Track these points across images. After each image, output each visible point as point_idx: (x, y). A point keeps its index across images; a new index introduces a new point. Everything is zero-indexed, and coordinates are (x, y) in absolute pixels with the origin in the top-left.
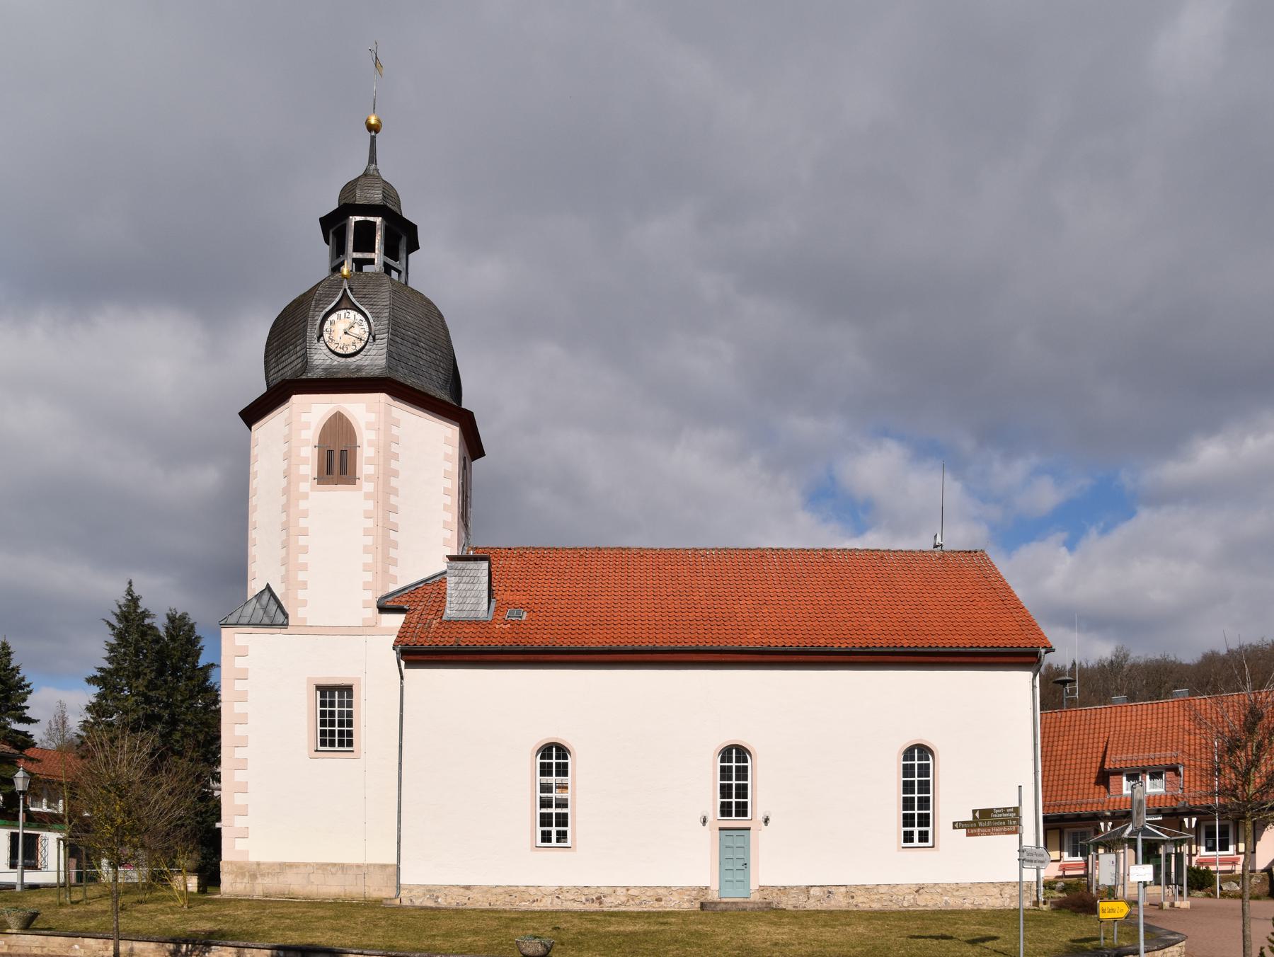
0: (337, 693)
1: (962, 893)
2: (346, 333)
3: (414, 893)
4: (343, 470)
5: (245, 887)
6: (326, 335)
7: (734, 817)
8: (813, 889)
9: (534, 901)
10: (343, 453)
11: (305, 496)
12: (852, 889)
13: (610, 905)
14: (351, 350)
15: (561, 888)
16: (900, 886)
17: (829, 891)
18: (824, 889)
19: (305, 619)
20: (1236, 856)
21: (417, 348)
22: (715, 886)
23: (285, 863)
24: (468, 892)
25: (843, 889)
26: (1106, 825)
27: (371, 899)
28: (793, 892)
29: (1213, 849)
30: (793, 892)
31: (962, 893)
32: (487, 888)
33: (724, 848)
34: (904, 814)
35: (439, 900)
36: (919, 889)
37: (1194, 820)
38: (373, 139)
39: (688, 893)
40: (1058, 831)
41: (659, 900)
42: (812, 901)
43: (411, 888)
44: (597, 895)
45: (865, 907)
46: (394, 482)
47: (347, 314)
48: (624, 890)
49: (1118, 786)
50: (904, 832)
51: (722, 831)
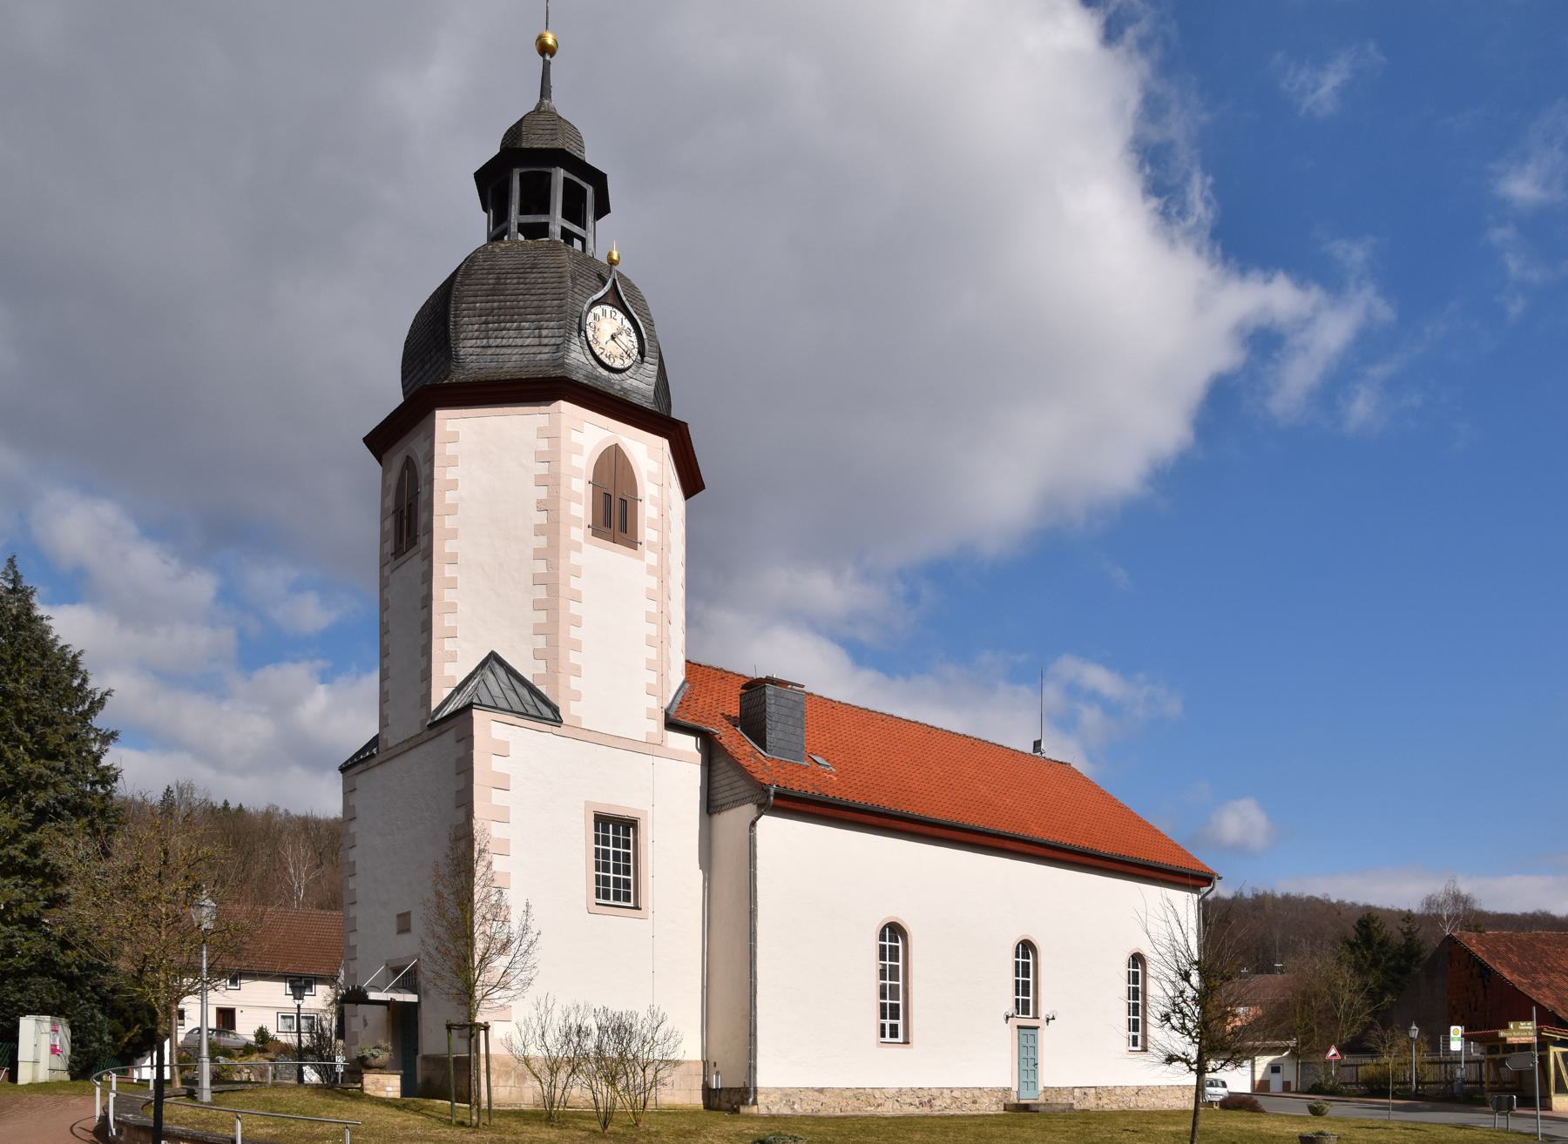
0: (611, 826)
3: (771, 1098)
5: (510, 1093)
9: (878, 1106)
11: (577, 547)
14: (618, 364)
15: (900, 1089)
27: (663, 1107)
32: (838, 1091)
33: (908, 1039)
35: (796, 1107)
36: (1139, 1091)
41: (974, 1102)
45: (1107, 1108)
47: (613, 314)
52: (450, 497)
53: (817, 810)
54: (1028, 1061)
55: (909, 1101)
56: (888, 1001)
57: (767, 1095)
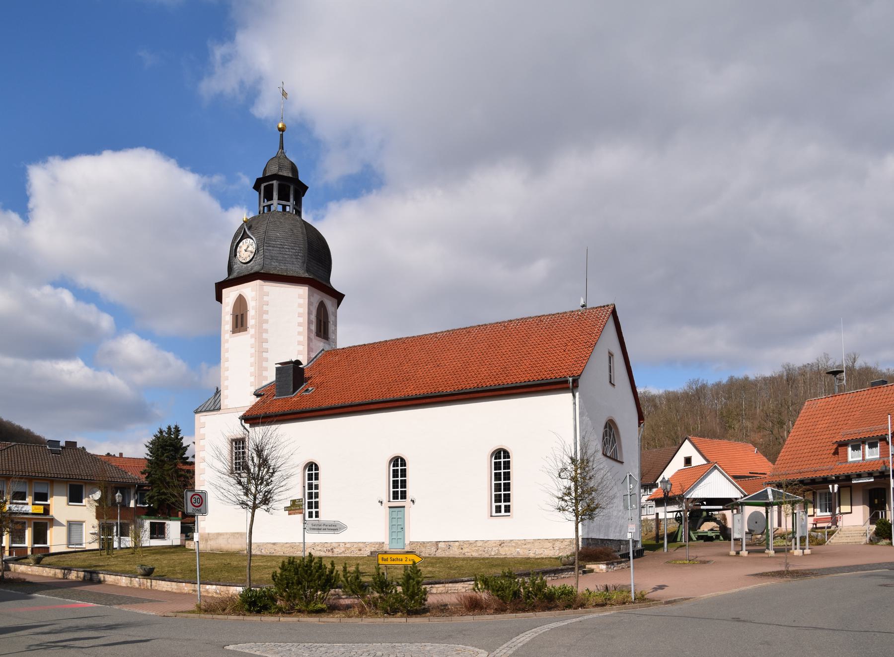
1: (528, 546)
2: (246, 251)
4: (242, 325)
6: (238, 254)
7: (399, 500)
8: (441, 543)
10: (242, 315)
12: (462, 544)
13: (337, 553)
15: (315, 543)
16: (490, 542)
17: (449, 544)
18: (446, 543)
19: (227, 405)
21: (283, 249)
22: (387, 541)
24: (274, 547)
25: (457, 544)
26: (833, 487)
28: (428, 545)
30: (428, 545)
31: (528, 546)
33: (392, 519)
34: (509, 491)
36: (501, 544)
38: (282, 136)
39: (374, 546)
40: (849, 488)
41: (360, 550)
42: (439, 551)
43: (259, 546)
44: (332, 547)
45: (468, 555)
46: (265, 326)
48: (343, 544)
49: (845, 455)
50: (496, 506)
51: (391, 509)
52: (301, 320)
53: (293, 416)
54: (397, 525)
56: (314, 500)
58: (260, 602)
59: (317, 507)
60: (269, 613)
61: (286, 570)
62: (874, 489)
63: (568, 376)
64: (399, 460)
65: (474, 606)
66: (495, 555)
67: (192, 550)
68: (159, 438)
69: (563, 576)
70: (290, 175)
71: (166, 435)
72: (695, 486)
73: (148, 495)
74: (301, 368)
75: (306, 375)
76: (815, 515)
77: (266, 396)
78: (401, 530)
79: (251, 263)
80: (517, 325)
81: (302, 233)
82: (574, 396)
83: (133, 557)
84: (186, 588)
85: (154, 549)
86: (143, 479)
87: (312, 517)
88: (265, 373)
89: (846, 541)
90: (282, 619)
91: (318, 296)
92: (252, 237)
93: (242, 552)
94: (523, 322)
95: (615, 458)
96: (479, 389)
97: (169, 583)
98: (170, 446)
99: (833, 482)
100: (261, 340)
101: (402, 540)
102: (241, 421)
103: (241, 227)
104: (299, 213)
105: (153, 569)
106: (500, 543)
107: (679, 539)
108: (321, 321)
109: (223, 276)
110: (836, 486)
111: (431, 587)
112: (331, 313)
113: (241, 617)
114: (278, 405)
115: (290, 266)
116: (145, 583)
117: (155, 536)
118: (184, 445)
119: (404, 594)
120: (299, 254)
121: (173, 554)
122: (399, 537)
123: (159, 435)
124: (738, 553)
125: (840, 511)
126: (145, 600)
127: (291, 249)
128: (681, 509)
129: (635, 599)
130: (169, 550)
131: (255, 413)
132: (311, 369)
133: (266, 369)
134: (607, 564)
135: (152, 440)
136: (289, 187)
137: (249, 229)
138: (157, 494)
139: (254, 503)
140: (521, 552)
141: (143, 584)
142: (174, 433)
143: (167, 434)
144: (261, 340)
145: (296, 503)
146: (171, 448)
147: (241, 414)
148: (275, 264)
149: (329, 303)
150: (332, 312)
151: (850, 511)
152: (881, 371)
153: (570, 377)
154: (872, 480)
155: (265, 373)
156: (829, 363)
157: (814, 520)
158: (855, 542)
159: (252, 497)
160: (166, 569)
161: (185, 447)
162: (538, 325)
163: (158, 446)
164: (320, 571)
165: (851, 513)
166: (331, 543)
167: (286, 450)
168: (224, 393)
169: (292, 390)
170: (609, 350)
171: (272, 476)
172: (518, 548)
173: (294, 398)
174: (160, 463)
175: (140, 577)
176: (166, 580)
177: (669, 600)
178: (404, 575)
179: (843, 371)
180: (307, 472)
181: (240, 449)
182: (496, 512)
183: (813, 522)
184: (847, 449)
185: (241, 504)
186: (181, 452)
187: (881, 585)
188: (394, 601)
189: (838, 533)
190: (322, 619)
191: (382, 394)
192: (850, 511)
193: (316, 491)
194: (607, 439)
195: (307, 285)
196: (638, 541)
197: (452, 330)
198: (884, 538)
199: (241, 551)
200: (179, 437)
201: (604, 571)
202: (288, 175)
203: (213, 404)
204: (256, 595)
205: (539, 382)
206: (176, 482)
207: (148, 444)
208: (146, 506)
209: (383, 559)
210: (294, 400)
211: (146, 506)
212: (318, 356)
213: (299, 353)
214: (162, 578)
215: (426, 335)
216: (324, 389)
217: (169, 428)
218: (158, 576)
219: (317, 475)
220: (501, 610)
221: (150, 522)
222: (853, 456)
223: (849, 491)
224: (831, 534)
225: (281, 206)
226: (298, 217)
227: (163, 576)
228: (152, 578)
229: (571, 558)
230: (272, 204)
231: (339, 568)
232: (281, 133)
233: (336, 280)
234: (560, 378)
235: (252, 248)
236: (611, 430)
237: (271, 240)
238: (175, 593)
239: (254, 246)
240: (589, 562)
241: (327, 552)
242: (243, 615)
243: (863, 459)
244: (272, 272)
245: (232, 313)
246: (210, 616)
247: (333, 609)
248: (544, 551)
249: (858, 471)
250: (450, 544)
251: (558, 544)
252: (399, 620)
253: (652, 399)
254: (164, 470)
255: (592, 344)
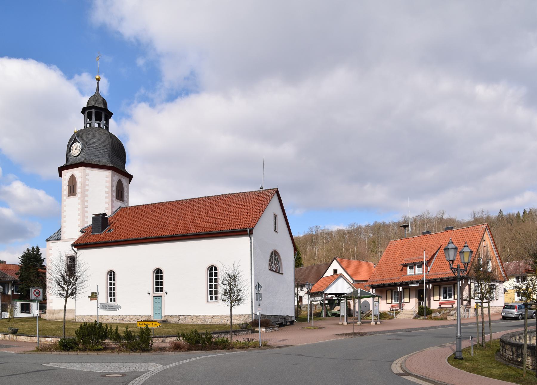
2: (76, 149)
3: (79, 318)
4: (73, 192)
6: (71, 151)
8: (181, 316)
15: (113, 316)
16: (207, 316)
17: (185, 317)
19: (65, 237)
20: (454, 301)
22: (152, 315)
23: (60, 310)
24: (91, 317)
25: (190, 317)
26: (400, 288)
29: (446, 298)
33: (155, 303)
36: (213, 317)
37: (431, 285)
38: (98, 83)
40: (409, 289)
42: (180, 320)
43: (78, 316)
45: (196, 323)
46: (86, 193)
48: (129, 316)
52: (107, 190)
54: (158, 306)
55: (116, 319)
56: (113, 292)
57: (78, 317)
58: (69, 345)
59: (114, 296)
60: (74, 351)
61: (82, 329)
62: (420, 290)
63: (247, 228)
64: (159, 270)
65: (177, 347)
66: (209, 323)
67: (45, 319)
68: (27, 253)
69: (239, 334)
70: (103, 107)
71: (31, 252)
72: (330, 287)
73: (20, 287)
74: (106, 217)
75: (109, 221)
76: (440, 300)
77: (87, 233)
78: (160, 309)
79: (79, 156)
80: (226, 198)
81: (109, 140)
82: (251, 238)
83: (8, 324)
84: (35, 340)
85: (22, 319)
86: (17, 278)
87: (112, 301)
88: (86, 220)
89: (404, 317)
90: (79, 353)
91: (117, 177)
92: (79, 141)
93: (73, 321)
94: (229, 196)
95: (278, 271)
96: (201, 233)
97: (26, 337)
98: (34, 259)
99: (399, 286)
100: (84, 201)
101: (160, 314)
102: (72, 247)
103: (73, 136)
104: (107, 128)
105: (18, 330)
106: (212, 317)
107: (322, 316)
108: (119, 190)
109: (63, 163)
110: (401, 288)
111: (165, 339)
112: (125, 186)
113: (59, 353)
114: (94, 238)
115: (101, 159)
116: (13, 337)
117: (24, 311)
118: (42, 258)
119: (140, 341)
120: (107, 152)
121: (33, 322)
122: (159, 313)
123: (27, 252)
124: (376, 323)
125: (404, 301)
126: (11, 346)
127: (102, 149)
128: (322, 299)
129: (261, 345)
130: (31, 319)
131: (79, 242)
132: (113, 218)
133: (87, 217)
134: (266, 328)
135: (22, 255)
136: (102, 113)
137: (78, 137)
138: (25, 287)
139: (67, 295)
140: (223, 321)
141: (12, 338)
142: (36, 251)
143: (31, 251)
144: (84, 201)
145: (94, 294)
146: (34, 260)
147: (72, 242)
148: (92, 158)
149: (124, 181)
150: (126, 185)
151: (409, 301)
152: (459, 221)
153: (248, 228)
154: (418, 285)
155: (86, 220)
156: (429, 216)
157: (392, 306)
158: (408, 318)
159: (66, 292)
160: (26, 330)
161: (43, 259)
162: (236, 198)
163: (26, 258)
164: (100, 329)
165: (409, 302)
166: (123, 316)
167: (83, 268)
168: (63, 230)
169: (101, 230)
170: (274, 213)
171: (76, 281)
172: (222, 319)
173: (102, 234)
174: (28, 269)
175: (10, 334)
176: (25, 335)
177: (278, 346)
178: (140, 331)
179: (409, 226)
180: (109, 276)
181: (72, 262)
182: (211, 300)
183: (391, 307)
184: (407, 268)
185: (59, 295)
186: (40, 262)
187: (389, 339)
188: (135, 344)
189: (401, 313)
190: (99, 353)
191: (150, 234)
192: (409, 301)
193: (114, 287)
194: (273, 261)
195: (111, 170)
196: (293, 316)
197: (191, 199)
198: (422, 316)
199: (72, 320)
200: (39, 254)
201: (264, 332)
202: (101, 107)
203: (57, 237)
204: (67, 341)
205: (232, 230)
206: (37, 280)
207: (20, 257)
208: (19, 293)
209: (140, 324)
210: (103, 235)
211: (19, 293)
212: (117, 211)
213: (106, 208)
214: (23, 335)
215: (177, 201)
216: (119, 230)
217: (33, 248)
218: (21, 334)
219: (114, 278)
220: (189, 349)
221: (21, 303)
222: (410, 272)
223: (409, 291)
224: (397, 313)
225: (98, 124)
226: (106, 131)
227: (24, 333)
228: (16, 334)
229: (244, 325)
230: (92, 123)
231: (114, 328)
232: (98, 81)
233: (129, 168)
234: (243, 228)
235: (80, 148)
236: (275, 257)
237: (90, 144)
238: (29, 342)
239: (81, 147)
240: (256, 327)
241: (120, 321)
242: (60, 352)
243: (415, 274)
244: (90, 163)
245: (67, 185)
246: (43, 352)
247: (106, 349)
248: (235, 321)
249: (411, 280)
250: (186, 317)
251: (242, 318)
252: (137, 354)
253: (299, 238)
254: (30, 273)
255: (262, 210)
